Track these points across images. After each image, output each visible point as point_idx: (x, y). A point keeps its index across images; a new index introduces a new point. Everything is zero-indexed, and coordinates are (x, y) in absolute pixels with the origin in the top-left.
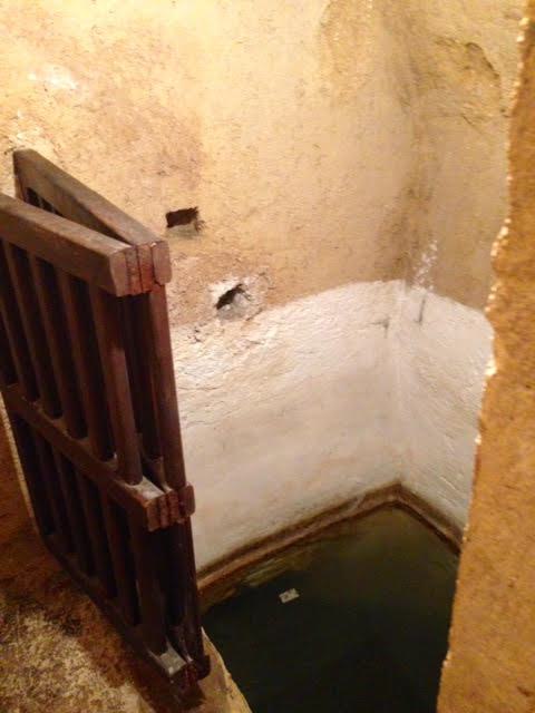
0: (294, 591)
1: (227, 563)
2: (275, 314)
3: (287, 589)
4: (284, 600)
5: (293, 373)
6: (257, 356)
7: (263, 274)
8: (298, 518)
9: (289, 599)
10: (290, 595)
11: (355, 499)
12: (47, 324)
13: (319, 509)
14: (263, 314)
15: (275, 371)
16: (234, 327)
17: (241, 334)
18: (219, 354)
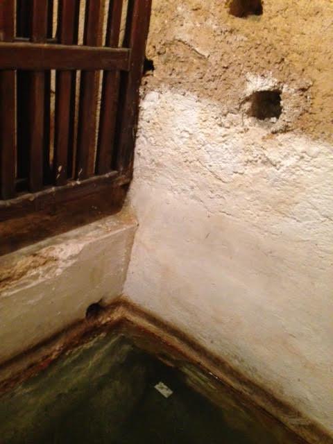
0: (170, 392)
1: (168, 332)
2: (299, 144)
3: (170, 387)
4: (157, 387)
5: (300, 225)
6: (267, 177)
7: (303, 90)
8: (235, 363)
9: (161, 391)
10: (164, 390)
11: (299, 414)
12: (76, 118)
13: (260, 381)
14: (287, 135)
15: (281, 207)
16: (257, 131)
17: (261, 143)
18: (236, 151)
